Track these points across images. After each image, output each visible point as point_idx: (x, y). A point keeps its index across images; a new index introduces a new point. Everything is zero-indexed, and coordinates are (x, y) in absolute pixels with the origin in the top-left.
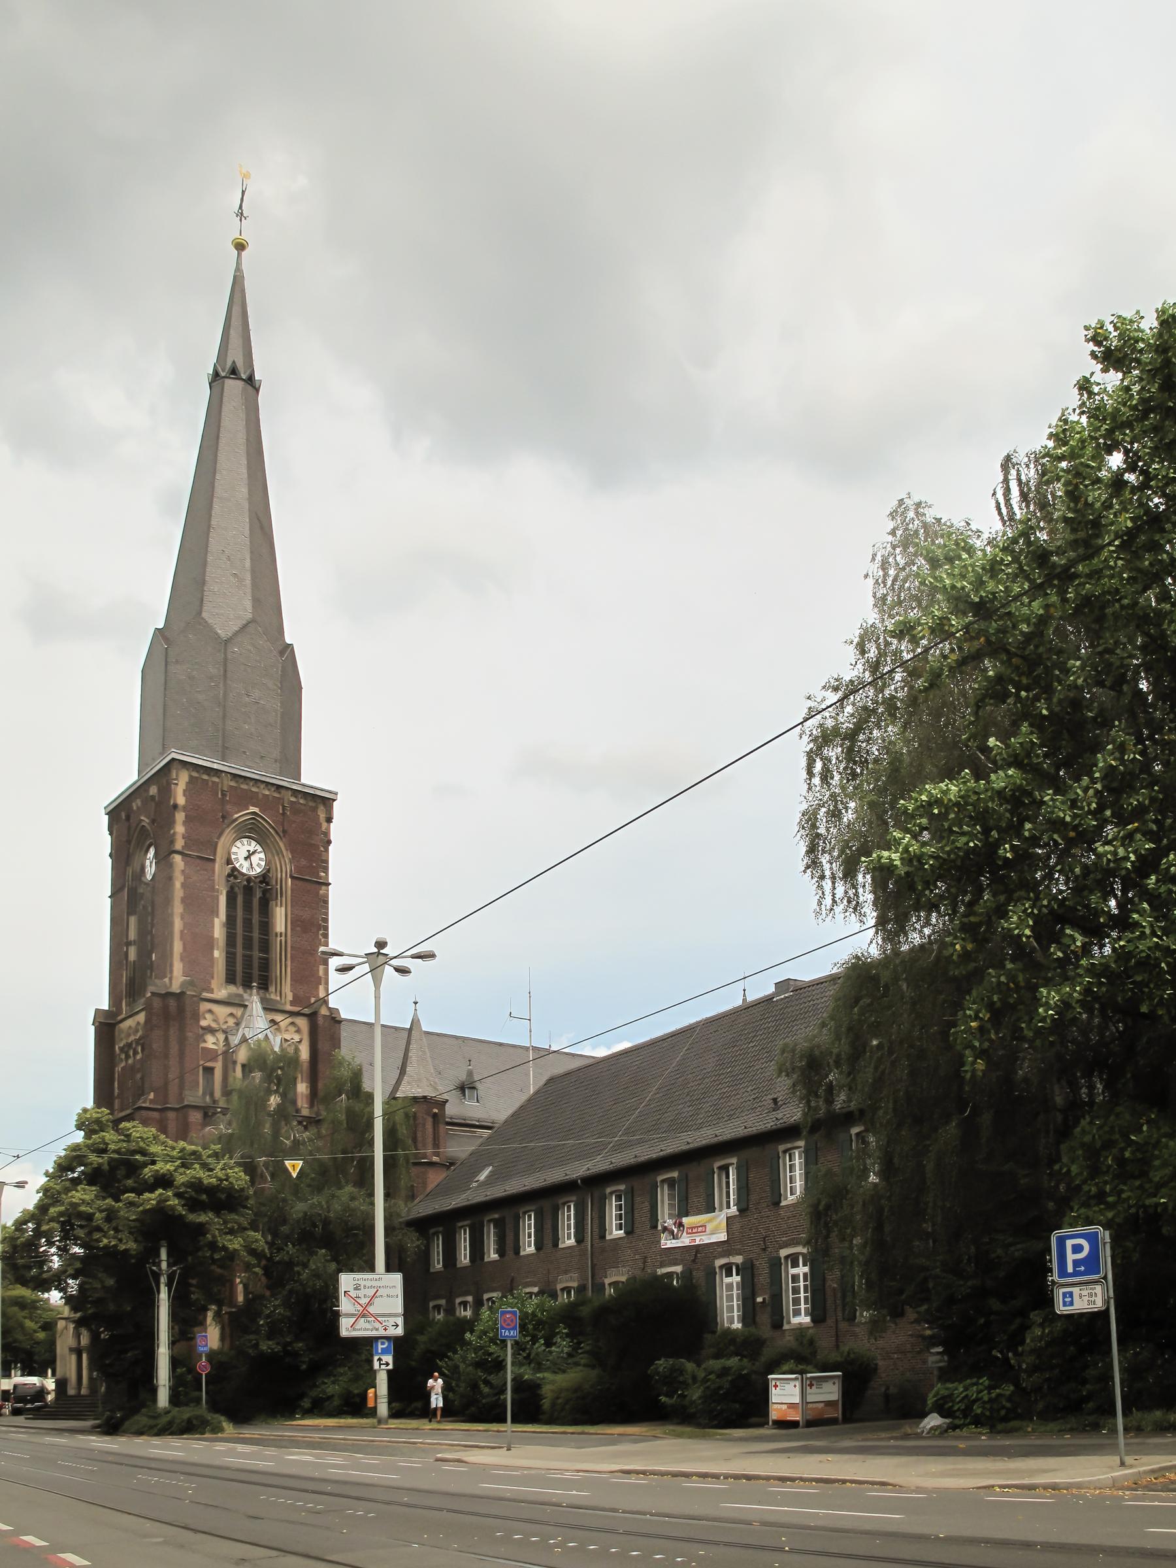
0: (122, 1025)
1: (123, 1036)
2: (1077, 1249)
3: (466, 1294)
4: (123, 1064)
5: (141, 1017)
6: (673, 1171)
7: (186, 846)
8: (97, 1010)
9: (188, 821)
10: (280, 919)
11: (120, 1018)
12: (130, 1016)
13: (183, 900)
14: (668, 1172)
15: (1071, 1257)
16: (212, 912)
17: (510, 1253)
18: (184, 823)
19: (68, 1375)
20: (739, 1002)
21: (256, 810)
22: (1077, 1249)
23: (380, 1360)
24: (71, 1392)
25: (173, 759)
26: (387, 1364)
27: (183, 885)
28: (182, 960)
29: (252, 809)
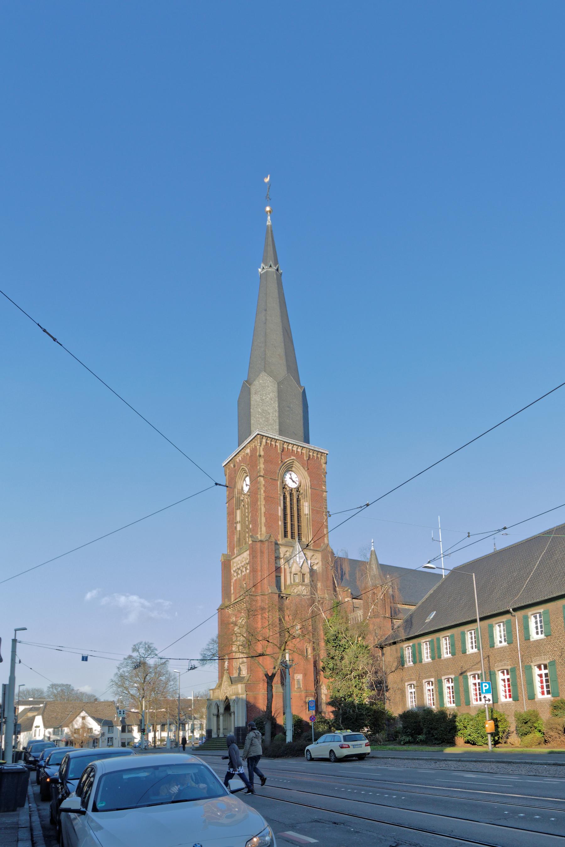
0: (234, 560)
1: (235, 565)
2: (486, 686)
3: (431, 677)
4: (235, 579)
5: (246, 554)
6: (540, 609)
7: (265, 474)
8: (223, 554)
9: (265, 462)
10: (306, 508)
11: (233, 557)
12: (239, 555)
13: (265, 499)
14: (538, 609)
15: (484, 688)
16: (278, 504)
17: (459, 654)
18: (264, 464)
19: (212, 728)
20: (492, 551)
21: (294, 458)
22: (486, 686)
23: (485, 697)
24: (214, 735)
25: (258, 434)
26: (489, 700)
27: (264, 491)
28: (265, 526)
29: (292, 458)
